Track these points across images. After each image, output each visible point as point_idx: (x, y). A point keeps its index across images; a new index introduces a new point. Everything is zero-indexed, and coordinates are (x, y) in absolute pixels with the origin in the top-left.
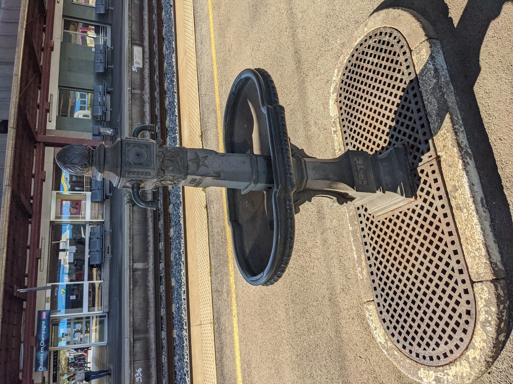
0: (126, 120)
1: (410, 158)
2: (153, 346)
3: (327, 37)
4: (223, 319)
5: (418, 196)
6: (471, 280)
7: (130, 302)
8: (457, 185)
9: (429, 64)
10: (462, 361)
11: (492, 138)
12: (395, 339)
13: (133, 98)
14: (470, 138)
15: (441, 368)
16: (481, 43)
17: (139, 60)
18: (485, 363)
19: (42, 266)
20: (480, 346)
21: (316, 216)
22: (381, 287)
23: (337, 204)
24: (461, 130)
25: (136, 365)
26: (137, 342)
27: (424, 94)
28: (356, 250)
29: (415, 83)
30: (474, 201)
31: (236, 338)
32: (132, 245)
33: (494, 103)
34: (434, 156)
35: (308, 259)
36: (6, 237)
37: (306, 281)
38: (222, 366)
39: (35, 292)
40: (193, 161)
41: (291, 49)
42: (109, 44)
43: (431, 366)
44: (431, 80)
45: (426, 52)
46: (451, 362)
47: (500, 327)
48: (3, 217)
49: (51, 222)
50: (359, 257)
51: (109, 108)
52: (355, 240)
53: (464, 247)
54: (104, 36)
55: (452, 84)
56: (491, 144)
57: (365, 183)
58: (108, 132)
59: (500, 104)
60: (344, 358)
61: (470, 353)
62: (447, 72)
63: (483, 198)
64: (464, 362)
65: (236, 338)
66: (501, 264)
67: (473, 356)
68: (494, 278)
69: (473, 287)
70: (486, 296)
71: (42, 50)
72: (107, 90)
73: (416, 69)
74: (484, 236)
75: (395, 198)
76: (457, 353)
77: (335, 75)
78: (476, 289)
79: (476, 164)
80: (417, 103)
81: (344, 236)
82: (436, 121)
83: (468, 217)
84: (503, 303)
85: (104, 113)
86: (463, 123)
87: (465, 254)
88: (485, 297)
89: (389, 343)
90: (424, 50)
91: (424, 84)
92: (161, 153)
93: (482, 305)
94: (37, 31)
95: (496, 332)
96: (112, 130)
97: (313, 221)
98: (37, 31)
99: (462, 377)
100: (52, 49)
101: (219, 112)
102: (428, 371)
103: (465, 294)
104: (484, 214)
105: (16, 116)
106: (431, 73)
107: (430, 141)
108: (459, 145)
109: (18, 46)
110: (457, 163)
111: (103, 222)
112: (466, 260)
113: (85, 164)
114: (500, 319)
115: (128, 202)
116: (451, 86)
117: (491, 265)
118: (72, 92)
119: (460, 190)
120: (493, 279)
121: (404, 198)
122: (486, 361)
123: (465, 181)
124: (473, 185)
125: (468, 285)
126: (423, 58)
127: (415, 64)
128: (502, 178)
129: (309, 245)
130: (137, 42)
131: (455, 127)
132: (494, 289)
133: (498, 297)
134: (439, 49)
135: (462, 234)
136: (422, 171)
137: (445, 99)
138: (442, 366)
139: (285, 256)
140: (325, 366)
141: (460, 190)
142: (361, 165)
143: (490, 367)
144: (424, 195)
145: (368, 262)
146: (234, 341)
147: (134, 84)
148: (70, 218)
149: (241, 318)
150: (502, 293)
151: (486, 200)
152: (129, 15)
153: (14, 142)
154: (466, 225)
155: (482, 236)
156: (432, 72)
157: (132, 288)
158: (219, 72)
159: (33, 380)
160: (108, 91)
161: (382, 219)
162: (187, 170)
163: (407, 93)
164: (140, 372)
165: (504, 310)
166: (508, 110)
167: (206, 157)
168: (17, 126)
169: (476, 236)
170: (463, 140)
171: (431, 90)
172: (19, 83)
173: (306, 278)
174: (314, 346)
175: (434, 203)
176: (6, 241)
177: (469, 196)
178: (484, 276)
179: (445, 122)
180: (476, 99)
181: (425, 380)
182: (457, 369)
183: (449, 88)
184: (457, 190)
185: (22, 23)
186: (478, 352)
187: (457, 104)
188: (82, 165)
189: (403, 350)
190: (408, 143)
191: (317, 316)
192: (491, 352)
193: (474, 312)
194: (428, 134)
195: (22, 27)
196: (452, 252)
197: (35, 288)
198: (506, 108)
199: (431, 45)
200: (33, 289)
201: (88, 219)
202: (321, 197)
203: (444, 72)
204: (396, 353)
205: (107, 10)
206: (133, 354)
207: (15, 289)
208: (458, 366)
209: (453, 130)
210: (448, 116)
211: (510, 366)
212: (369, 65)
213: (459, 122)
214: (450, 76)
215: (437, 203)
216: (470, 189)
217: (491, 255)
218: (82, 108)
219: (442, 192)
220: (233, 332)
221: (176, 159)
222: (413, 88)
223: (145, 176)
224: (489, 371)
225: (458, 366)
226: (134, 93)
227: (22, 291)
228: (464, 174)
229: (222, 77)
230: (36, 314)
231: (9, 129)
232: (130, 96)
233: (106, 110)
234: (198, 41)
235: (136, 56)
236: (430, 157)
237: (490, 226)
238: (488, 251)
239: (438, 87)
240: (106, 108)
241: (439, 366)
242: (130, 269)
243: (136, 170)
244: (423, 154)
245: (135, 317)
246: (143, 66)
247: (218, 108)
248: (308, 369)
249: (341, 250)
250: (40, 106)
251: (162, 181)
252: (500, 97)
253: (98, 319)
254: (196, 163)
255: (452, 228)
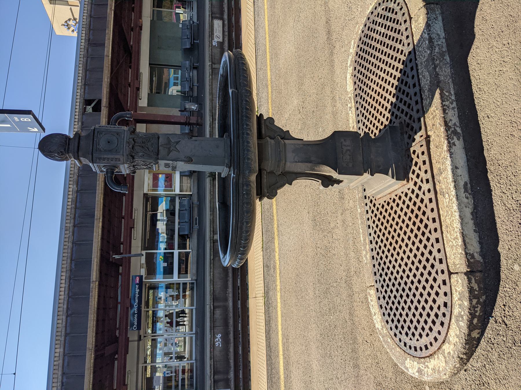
0: (207, 95)
1: (406, 136)
2: (231, 315)
3: (351, 4)
4: (271, 293)
5: (410, 179)
6: (449, 271)
7: (210, 271)
8: (442, 168)
9: (425, 33)
10: (439, 355)
11: (481, 115)
12: (389, 326)
13: (213, 73)
14: (461, 115)
15: (422, 360)
16: (476, 7)
17: (219, 34)
18: (458, 359)
19: (135, 235)
20: (453, 340)
21: (338, 197)
22: (380, 272)
23: (322, 187)
24: (451, 106)
25: (215, 330)
26: (217, 309)
27: (419, 67)
28: (363, 232)
29: (413, 53)
30: (455, 185)
31: (279, 313)
32: (212, 217)
33: (485, 76)
34: (425, 136)
35: (331, 240)
36: (102, 208)
37: (329, 262)
38: (270, 338)
39: (129, 259)
40: (164, 146)
41: (324, 19)
42: (195, 20)
43: (415, 357)
44: (425, 52)
45: (423, 20)
46: (431, 355)
47: (473, 323)
48: (99, 190)
49: (144, 194)
50: (364, 240)
51: (196, 84)
52: (362, 222)
53: (444, 236)
54: (190, 11)
55: (449, 54)
56: (480, 122)
57: (351, 165)
58: (193, 107)
59: (491, 76)
60: (355, 340)
61: (446, 347)
62: (444, 41)
63: (468, 183)
64: (441, 356)
65: (279, 313)
66: (480, 255)
67: (448, 351)
68: (469, 270)
69: (450, 279)
70: (460, 288)
71: (132, 29)
72: (193, 65)
73: (414, 39)
74: (461, 224)
75: (387, 181)
76: (436, 345)
77: (352, 47)
78: (452, 280)
79: (465, 145)
80: (413, 77)
82: (428, 97)
83: (449, 203)
84: (477, 297)
85: (191, 89)
86: (455, 98)
87: (445, 242)
88: (460, 289)
89: (384, 329)
90: (421, 17)
91: (419, 56)
92: (131, 140)
93: (457, 299)
94: (127, 11)
95: (467, 328)
96: (196, 106)
97: (335, 201)
98: (127, 11)
99: (439, 372)
100: (141, 28)
102: (413, 362)
103: (443, 285)
104: (466, 200)
105: (108, 95)
106: (426, 43)
107: (422, 119)
108: (446, 124)
109: (108, 27)
110: (443, 143)
111: (191, 195)
112: (446, 249)
113: (61, 152)
114: (472, 315)
115: (209, 176)
116: (447, 58)
117: (466, 256)
118: (165, 70)
119: (444, 174)
120: (467, 271)
121: (394, 180)
122: (459, 357)
123: (449, 163)
124: (457, 168)
125: (446, 276)
126: (420, 26)
127: (414, 33)
128: (487, 161)
129: (332, 225)
130: (217, 15)
131: (444, 103)
132: (467, 282)
133: (471, 290)
134: (438, 15)
135: (443, 222)
136: (414, 152)
137: (436, 72)
138: (424, 358)
139: (242, 240)
140: (341, 347)
141: (444, 174)
142: (348, 146)
143: (466, 364)
144: (414, 177)
145: (371, 245)
146: (277, 315)
147: (214, 59)
148: (165, 191)
149: (283, 295)
150: (476, 287)
151: (471, 185)
153: (107, 120)
154: (447, 212)
155: (459, 224)
156: (427, 42)
157: (212, 258)
158: (271, 45)
159: (129, 338)
160: (194, 66)
161: (382, 202)
162: (158, 154)
163: (406, 66)
164: (220, 338)
165: (478, 305)
166: (496, 83)
167: (177, 143)
168: (110, 104)
169: (455, 224)
170: (452, 119)
171: (426, 63)
172: (110, 63)
173: (329, 258)
174: (333, 327)
175: (422, 187)
176: (101, 212)
177: (451, 180)
178: (459, 267)
179: (435, 98)
180: (469, 71)
181: (410, 370)
182: (435, 363)
183: (443, 59)
184: (442, 173)
185: (111, 5)
186: (452, 346)
187: (452, 77)
188: (58, 153)
189: (394, 337)
190: (405, 121)
191: (336, 298)
192: (464, 348)
193: (450, 305)
194: (421, 112)
195: (111, 9)
196: (435, 240)
197: (129, 255)
198: (495, 81)
199: (428, 12)
200: (127, 255)
201: (177, 191)
202: (305, 180)
203: (441, 42)
204: (389, 340)
206: (213, 320)
207: (111, 255)
208: (436, 359)
209: (442, 107)
210: (438, 91)
211: (484, 365)
212: (377, 35)
213: (450, 98)
214: (448, 45)
215: (425, 187)
216: (453, 172)
217: (467, 245)
218: (175, 84)
219: (429, 176)
220: (277, 305)
221: (147, 144)
222: (411, 61)
223: (115, 162)
224: (465, 368)
225: (436, 359)
226: (214, 68)
227: (117, 257)
228: (447, 156)
229: (272, 50)
230: (131, 278)
231: (102, 108)
232: (211, 71)
233: (193, 85)
234: (256, 13)
235: (216, 30)
236: (421, 136)
237: (472, 214)
238: (464, 241)
239: (432, 58)
240: (193, 84)
241: (422, 358)
242: (210, 240)
243: (105, 156)
244: (416, 133)
245: (215, 286)
246: (223, 39)
247: (269, 82)
248: (328, 348)
249: (355, 232)
250: (131, 84)
251: (136, 165)
252: (490, 68)
253: (191, 285)
254: (167, 148)
255: (435, 215)
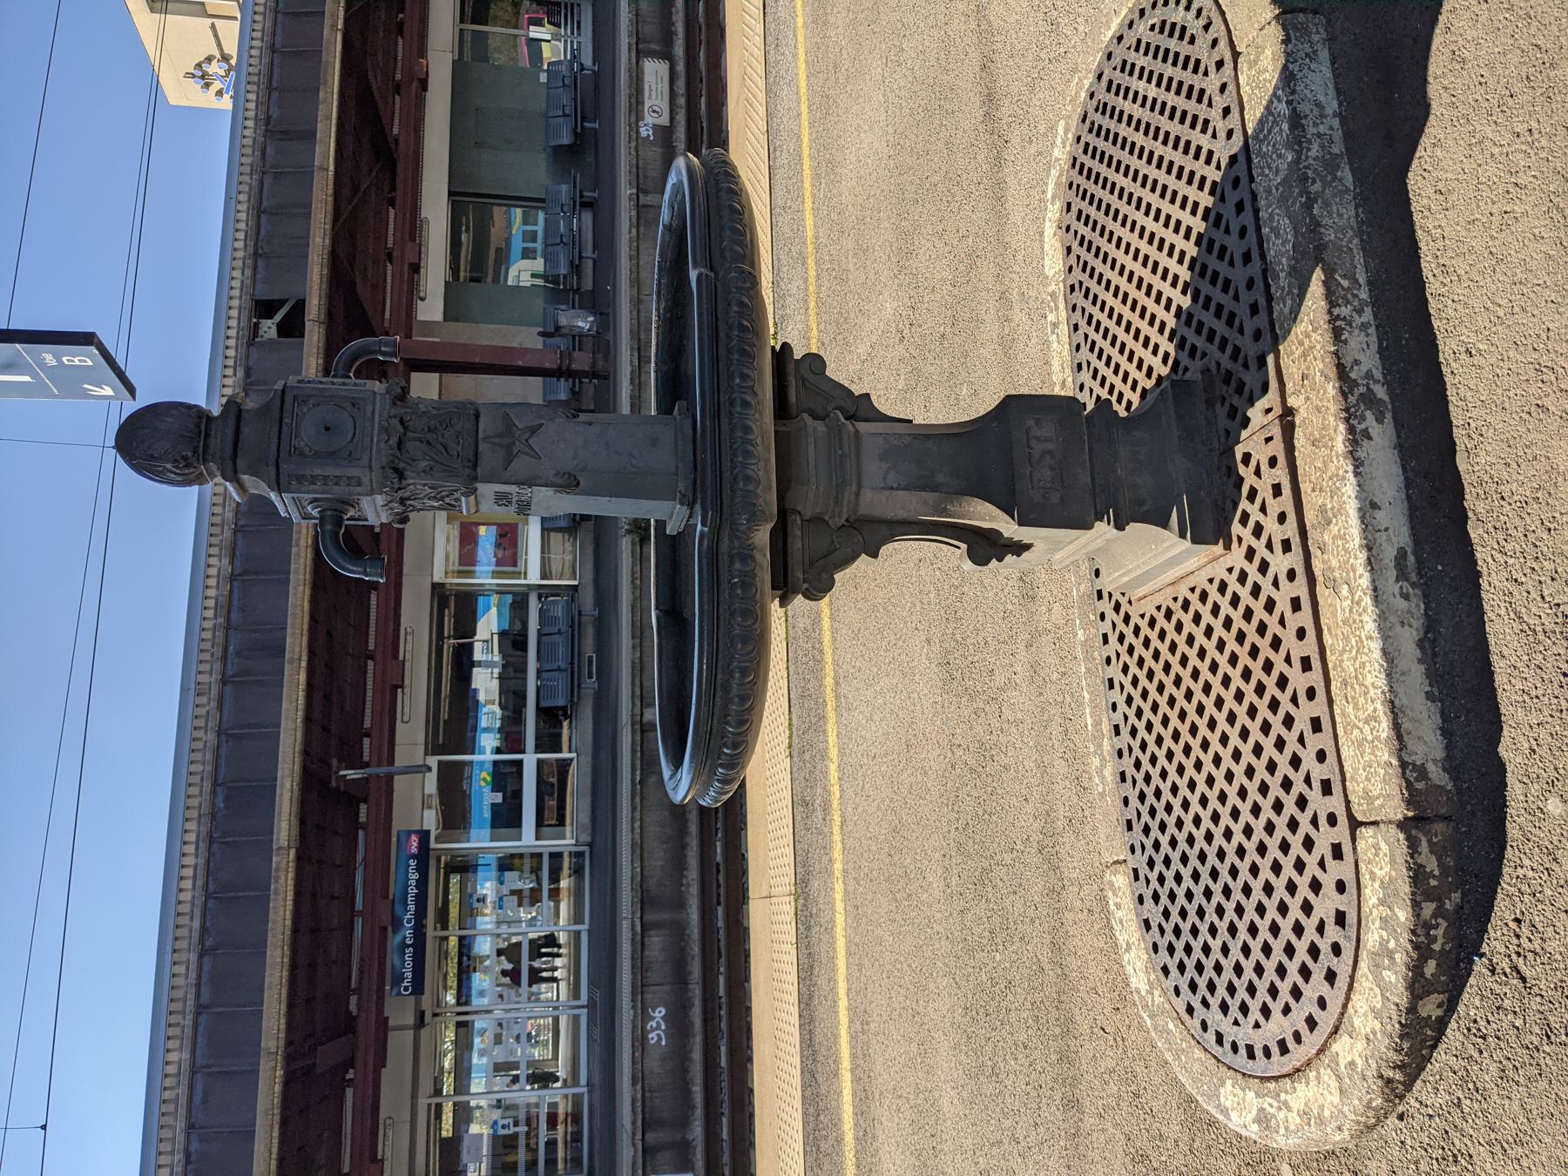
0: (623, 288)
1: (1222, 411)
2: (695, 949)
3: (1055, 13)
4: (815, 884)
5: (1235, 539)
6: (1350, 817)
7: (633, 818)
8: (1329, 506)
9: (1279, 100)
10: (1322, 1071)
11: (1447, 347)
12: (1169, 984)
13: (642, 222)
14: (1387, 348)
15: (1271, 1085)
16: (1434, 21)
17: (658, 102)
18: (1380, 1082)
19: (407, 710)
20: (1365, 1026)
21: (1017, 593)
22: (1143, 820)
23: (968, 565)
24: (1358, 320)
25: (648, 996)
26: (652, 932)
27: (1262, 203)
28: (1091, 701)
29: (1243, 161)
30: (1369, 559)
31: (841, 944)
32: (638, 655)
33: (1459, 228)
34: (1278, 411)
35: (996, 724)
36: (306, 627)
37: (989, 790)
38: (812, 1020)
39: (389, 781)
40: (494, 440)
41: (975, 57)
42: (587, 60)
43: (1250, 1076)
44: (1280, 156)
45: (1273, 59)
46: (1298, 1070)
47: (1422, 975)
48: (297, 572)
49: (435, 586)
50: (1097, 724)
51: (588, 252)
52: (1088, 670)
53: (1337, 711)
54: (572, 33)
55: (1351, 164)
56: (1444, 369)
57: (1055, 498)
58: (580, 324)
59: (1477, 230)
60: (1068, 1026)
61: (1341, 1045)
62: (1336, 123)
63: (1409, 550)
64: (1326, 1074)
65: (841, 944)
66: (1444, 770)
67: (1349, 1059)
68: (1410, 814)
69: (1354, 840)
70: (1383, 870)
71: (397, 89)
72: (581, 196)
73: (1246, 117)
74: (1389, 675)
75: (1165, 545)
76: (1312, 1041)
77: (1059, 141)
78: (1361, 845)
79: (1399, 437)
80: (1243, 232)
82: (1289, 293)
83: (1351, 611)
84: (1435, 896)
85: (576, 268)
86: (1371, 297)
87: (1340, 731)
88: (1383, 872)
89: (1157, 993)
90: (1268, 52)
91: (1262, 168)
92: (395, 422)
93: (1374, 900)
94: (381, 34)
95: (1407, 989)
96: (591, 319)
97: (1010, 607)
98: (381, 34)
99: (1321, 1121)
100: (424, 84)
102: (1244, 1090)
103: (1334, 858)
104: (1401, 604)
105: (324, 287)
106: (1281, 130)
107: (1270, 359)
108: (1342, 373)
109: (326, 82)
110: (1332, 432)
111: (575, 588)
112: (1342, 751)
113: (185, 458)
114: (1422, 950)
115: (629, 532)
116: (1346, 175)
117: (1404, 773)
118: (498, 212)
119: (1337, 524)
120: (1406, 818)
121: (1187, 544)
122: (1381, 1077)
123: (1350, 493)
124: (1374, 506)
125: (1341, 833)
126: (1265, 80)
127: (1245, 99)
128: (1466, 485)
129: (1000, 679)
130: (654, 46)
131: (1336, 311)
132: (1405, 850)
133: (1418, 876)
134: (1319, 47)
135: (1334, 669)
136: (1247, 458)
137: (1312, 217)
138: (1276, 1078)
139: (727, 723)
140: (1025, 1048)
141: (1337, 524)
142: (1047, 440)
143: (1401, 1097)
144: (1246, 533)
145: (1115, 740)
146: (834, 950)
147: (645, 177)
148: (496, 574)
149: (851, 888)
150: (1432, 865)
151: (1417, 558)
153: (321, 361)
154: (1346, 638)
155: (1383, 676)
156: (1285, 127)
157: (638, 778)
158: (814, 136)
159: (387, 1018)
160: (584, 199)
161: (1150, 610)
162: (475, 466)
163: (1222, 199)
164: (662, 1018)
165: (1440, 920)
166: (1494, 250)
167: (534, 430)
168: (330, 313)
169: (1369, 676)
170: (1361, 357)
171: (1281, 189)
172: (331, 191)
173: (990, 779)
174: (1003, 986)
175: (1271, 563)
176: (305, 638)
177: (1357, 541)
178: (1382, 806)
179: (1309, 295)
180: (1411, 213)
181: (1234, 1115)
182: (1310, 1094)
183: (1335, 177)
184: (1329, 523)
185: (335, 16)
186: (1361, 1045)
187: (1360, 233)
188: (176, 461)
189: (1186, 1017)
190: (1218, 364)
191: (1012, 897)
192: (1396, 1050)
193: (1355, 921)
194: (1267, 337)
195: (334, 26)
196: (1309, 722)
197: (389, 769)
198: (1490, 243)
199: (1288, 35)
200: (383, 770)
201: (534, 577)
202: (917, 543)
203: (1328, 127)
204: (1171, 1026)
206: (641, 966)
207: (334, 769)
208: (1313, 1083)
209: (1329, 322)
210: (1318, 276)
211: (1456, 1101)
212: (1136, 106)
213: (1356, 296)
214: (1348, 137)
215: (1280, 563)
216: (1362, 519)
217: (1406, 738)
218: (528, 254)
219: (1291, 530)
220: (832, 921)
221: (443, 435)
222: (1236, 183)
223: (347, 489)
224: (1400, 1109)
225: (1313, 1083)
226: (644, 206)
227: (352, 774)
228: (1347, 472)
229: (819, 151)
230: (394, 839)
231: (308, 325)
232: (634, 213)
233: (581, 257)
234: (769, 39)
235: (651, 90)
236: (1268, 411)
237: (1420, 644)
238: (1396, 726)
239: (1299, 176)
240: (580, 253)
241: (1269, 1079)
242: (633, 724)
243: (317, 472)
244: (1251, 402)
245: (646, 863)
246: (672, 119)
247: (810, 248)
248: (989, 1049)
249: (1068, 699)
250: (395, 254)
251: (408, 499)
252: (1474, 206)
253: (574, 860)
254: (501, 446)
255: (1309, 647)
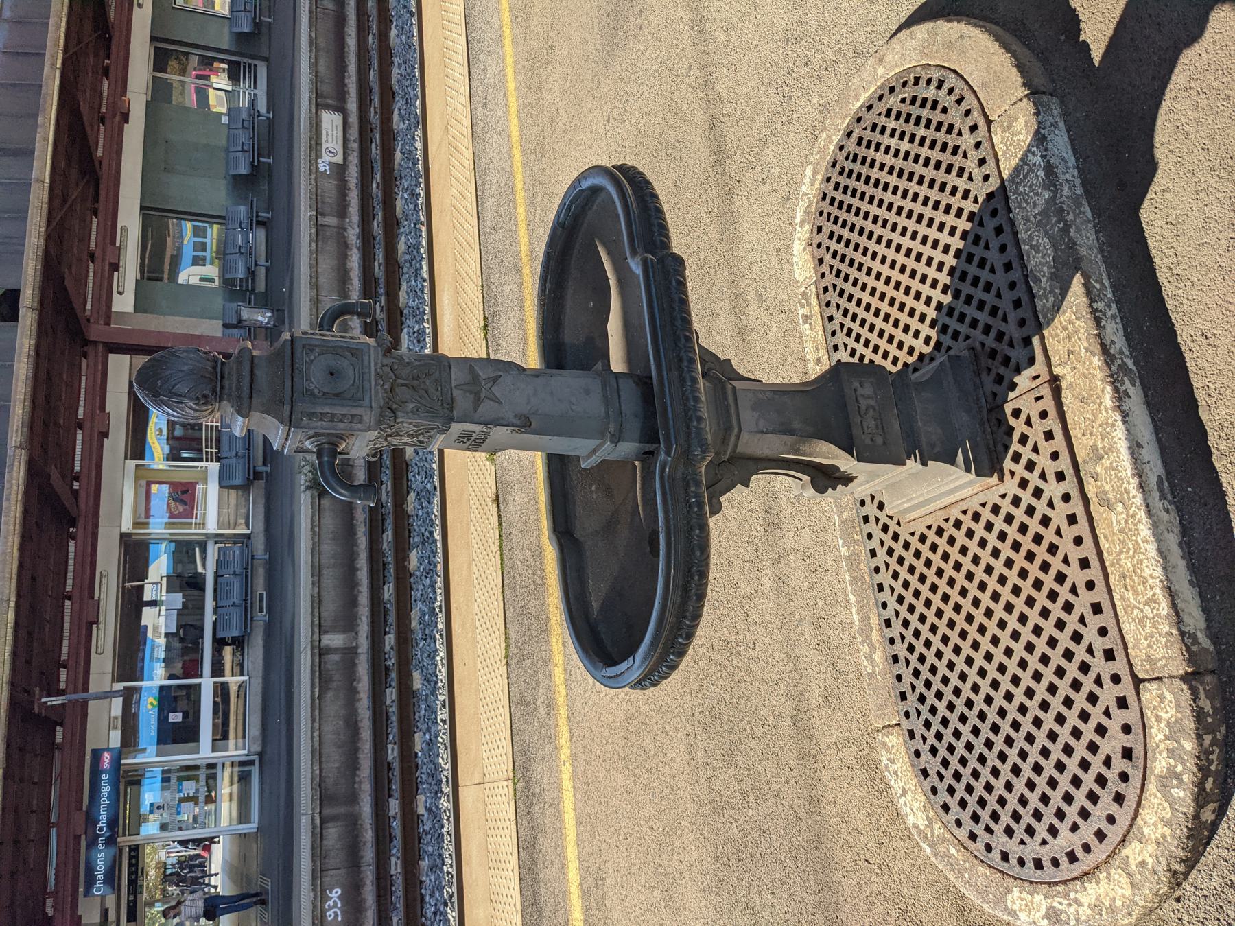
0: (302, 289)
1: (988, 380)
2: (368, 835)
3: (787, 89)
4: (537, 769)
5: (1007, 473)
6: (1134, 675)
7: (312, 728)
8: (1100, 446)
9: (1034, 154)
10: (1113, 871)
11: (1184, 334)
12: (951, 817)
13: (320, 237)
14: (1131, 333)
15: (1061, 888)
16: (1158, 104)
17: (334, 145)
18: (1169, 875)
19: (101, 642)
20: (1154, 833)
21: (762, 522)
22: (918, 691)
23: (811, 492)
24: (1109, 313)
25: (327, 880)
26: (330, 825)
27: (1021, 228)
28: (857, 602)
29: (998, 201)
30: (1140, 484)
31: (569, 815)
32: (317, 590)
33: (1190, 249)
34: (1045, 377)
35: (741, 626)
36: (15, 571)
37: (736, 679)
38: (535, 882)
39: (84, 705)
40: (464, 387)
41: (702, 118)
42: (262, 107)
43: (1036, 883)
44: (1037, 194)
45: (1026, 126)
46: (1086, 874)
47: (1204, 789)
48: (7, 523)
49: (123, 536)
50: (865, 620)
51: (262, 261)
52: (854, 578)
53: (1116, 597)
54: (250, 87)
55: (1088, 202)
56: (1183, 348)
57: (879, 440)
58: (260, 318)
59: (1205, 250)
60: (828, 862)
61: (1133, 851)
62: (1076, 173)
63: (1164, 478)
64: (1116, 874)
65: (569, 815)
66: (1207, 637)
67: (1140, 859)
68: (1190, 670)
69: (1138, 693)
70: (1169, 713)
71: (102, 120)
72: (257, 216)
73: (1002, 166)
74: (1165, 568)
75: (951, 478)
76: (1100, 851)
77: (807, 180)
78: (1145, 697)
79: (1146, 396)
80: (1003, 248)
81: (829, 568)
82: (1050, 292)
83: (1126, 522)
84: (1211, 730)
85: (252, 274)
86: (1114, 296)
87: (1120, 611)
88: (1169, 715)
89: (936, 827)
90: (1021, 121)
91: (1020, 203)
92: (387, 369)
93: (1161, 737)
94: (90, 75)
95: (1193, 801)
96: (269, 314)
97: (755, 533)
98: (90, 75)
99: (1112, 910)
100: (125, 118)
101: (526, 271)
102: (1031, 895)
103: (1119, 708)
104: (1165, 516)
105: (38, 279)
106: (1037, 176)
107: (1036, 341)
108: (1105, 350)
109: (44, 110)
110: (1099, 392)
111: (248, 536)
112: (1123, 626)
113: (205, 396)
114: (1204, 770)
115: (309, 488)
116: (1086, 208)
117: (1183, 640)
118: (172, 223)
119: (1109, 459)
120: (1187, 673)
121: (972, 476)
122: (1169, 870)
123: (1120, 436)
124: (1139, 446)
125: (1126, 688)
126: (1019, 140)
127: (1000, 153)
128: (1208, 430)
129: (745, 590)
130: (331, 102)
131: (1095, 305)
132: (1189, 697)
133: (1199, 715)
134: (1058, 119)
135: (1112, 565)
136: (1016, 413)
137: (1070, 239)
138: (1065, 882)
139: (685, 617)
140: (783, 884)
141: (1109, 459)
142: (869, 397)
143: (1179, 885)
144: (1020, 469)
145: (886, 631)
146: (562, 821)
147: (323, 202)
148: (169, 525)
149: (581, 768)
150: (1208, 707)
151: (1169, 483)
152: (310, 36)
153: (33, 342)
154: (1123, 543)
155: (1160, 569)
156: (1041, 173)
157: (317, 694)
158: (528, 173)
159: (80, 917)
160: (260, 219)
161: (920, 528)
162: (451, 409)
163: (981, 224)
164: (338, 897)
165: (1215, 748)
166: (1223, 264)
167: (495, 380)
168: (42, 303)
169: (1146, 569)
170: (1114, 339)
171: (1039, 218)
172: (46, 200)
173: (737, 670)
174: (756, 835)
175: (1045, 490)
176: (14, 582)
177: (1129, 472)
178: (1165, 665)
179: (1070, 293)
180: (1145, 239)
181: (1022, 916)
182: (1101, 891)
183: (1080, 211)
184: (1101, 458)
185: (54, 56)
186: (1151, 848)
187: (1101, 251)
188: (197, 398)
189: (969, 843)
190: (983, 345)
191: (764, 763)
192: (1183, 849)
193: (1142, 753)
194: (1030, 323)
195: (53, 65)
196: (1089, 607)
197: (84, 695)
198: (1219, 259)
199: (1037, 109)
200: (80, 696)
201: (212, 527)
202: (772, 476)
203: (1069, 175)
204: (953, 851)
205: (257, 25)
206: (319, 853)
207: (37, 696)
208: (1103, 882)
209: (1091, 313)
210: (1078, 280)
211: (1229, 883)
212: (888, 156)
213: (1105, 295)
214: (1084, 184)
215: (1053, 489)
216: (1132, 455)
217: (1181, 614)
218: (197, 261)
219: (1064, 464)
220: (560, 799)
221: (424, 382)
222: (994, 213)
223: (350, 425)
224: (1177, 894)
225: (1103, 882)
226: (321, 225)
227: (53, 701)
228: (1116, 421)
229: (533, 186)
230: (88, 757)
231: (22, 311)
232: (313, 231)
233: (256, 265)
234: (476, 99)
235: (327, 135)
236: (1035, 378)
237: (1180, 544)
238: (1174, 606)
239: (1055, 209)
240: (256, 261)
241: (1056, 883)
242: (313, 648)
243: (327, 410)
244: (1018, 371)
245: (324, 766)
246: (345, 159)
247: (525, 260)
248: (742, 889)
249: (820, 603)
250: (96, 255)
251: (391, 435)
252: (1203, 233)
253: (236, 769)
254: (471, 392)
255: (1088, 550)
